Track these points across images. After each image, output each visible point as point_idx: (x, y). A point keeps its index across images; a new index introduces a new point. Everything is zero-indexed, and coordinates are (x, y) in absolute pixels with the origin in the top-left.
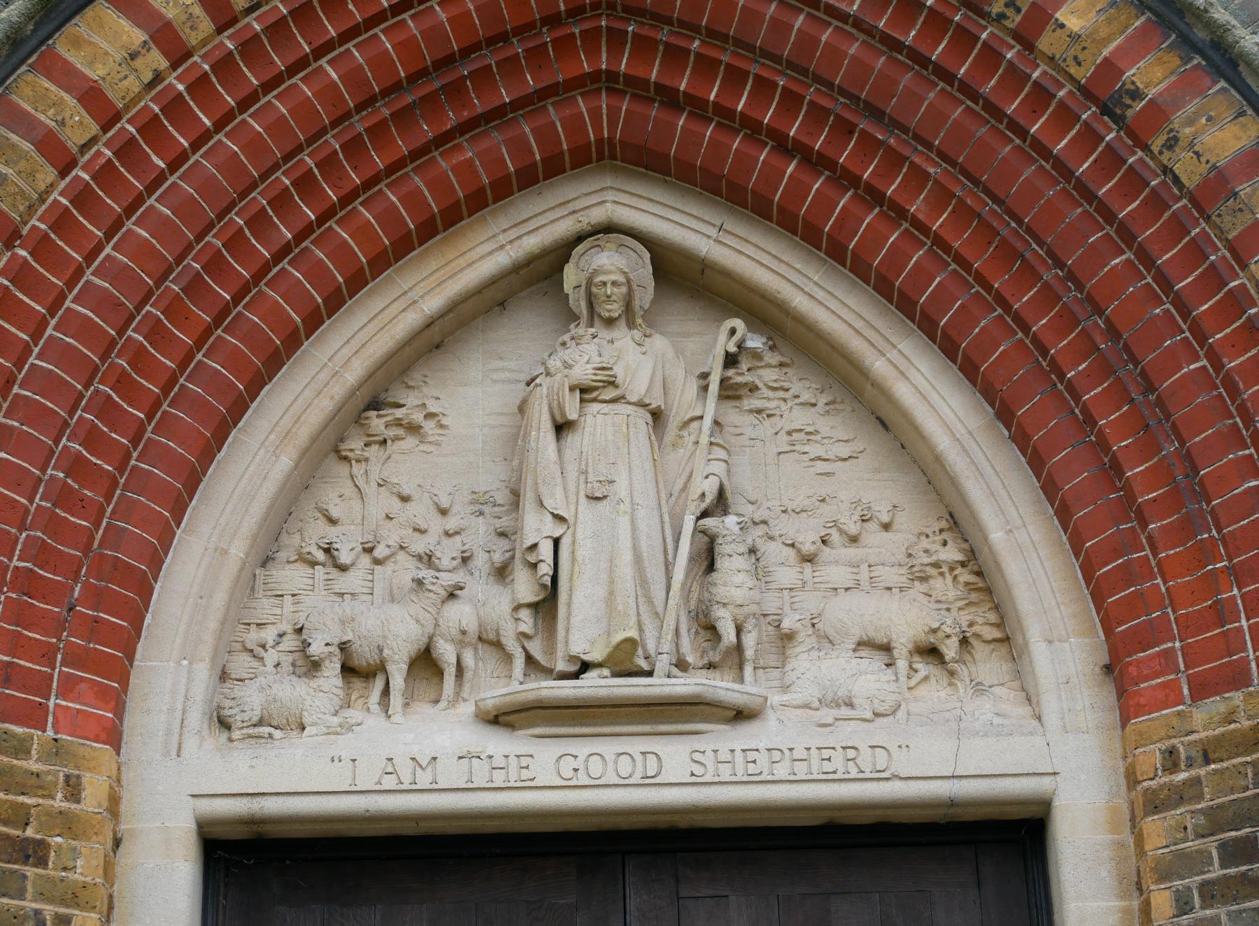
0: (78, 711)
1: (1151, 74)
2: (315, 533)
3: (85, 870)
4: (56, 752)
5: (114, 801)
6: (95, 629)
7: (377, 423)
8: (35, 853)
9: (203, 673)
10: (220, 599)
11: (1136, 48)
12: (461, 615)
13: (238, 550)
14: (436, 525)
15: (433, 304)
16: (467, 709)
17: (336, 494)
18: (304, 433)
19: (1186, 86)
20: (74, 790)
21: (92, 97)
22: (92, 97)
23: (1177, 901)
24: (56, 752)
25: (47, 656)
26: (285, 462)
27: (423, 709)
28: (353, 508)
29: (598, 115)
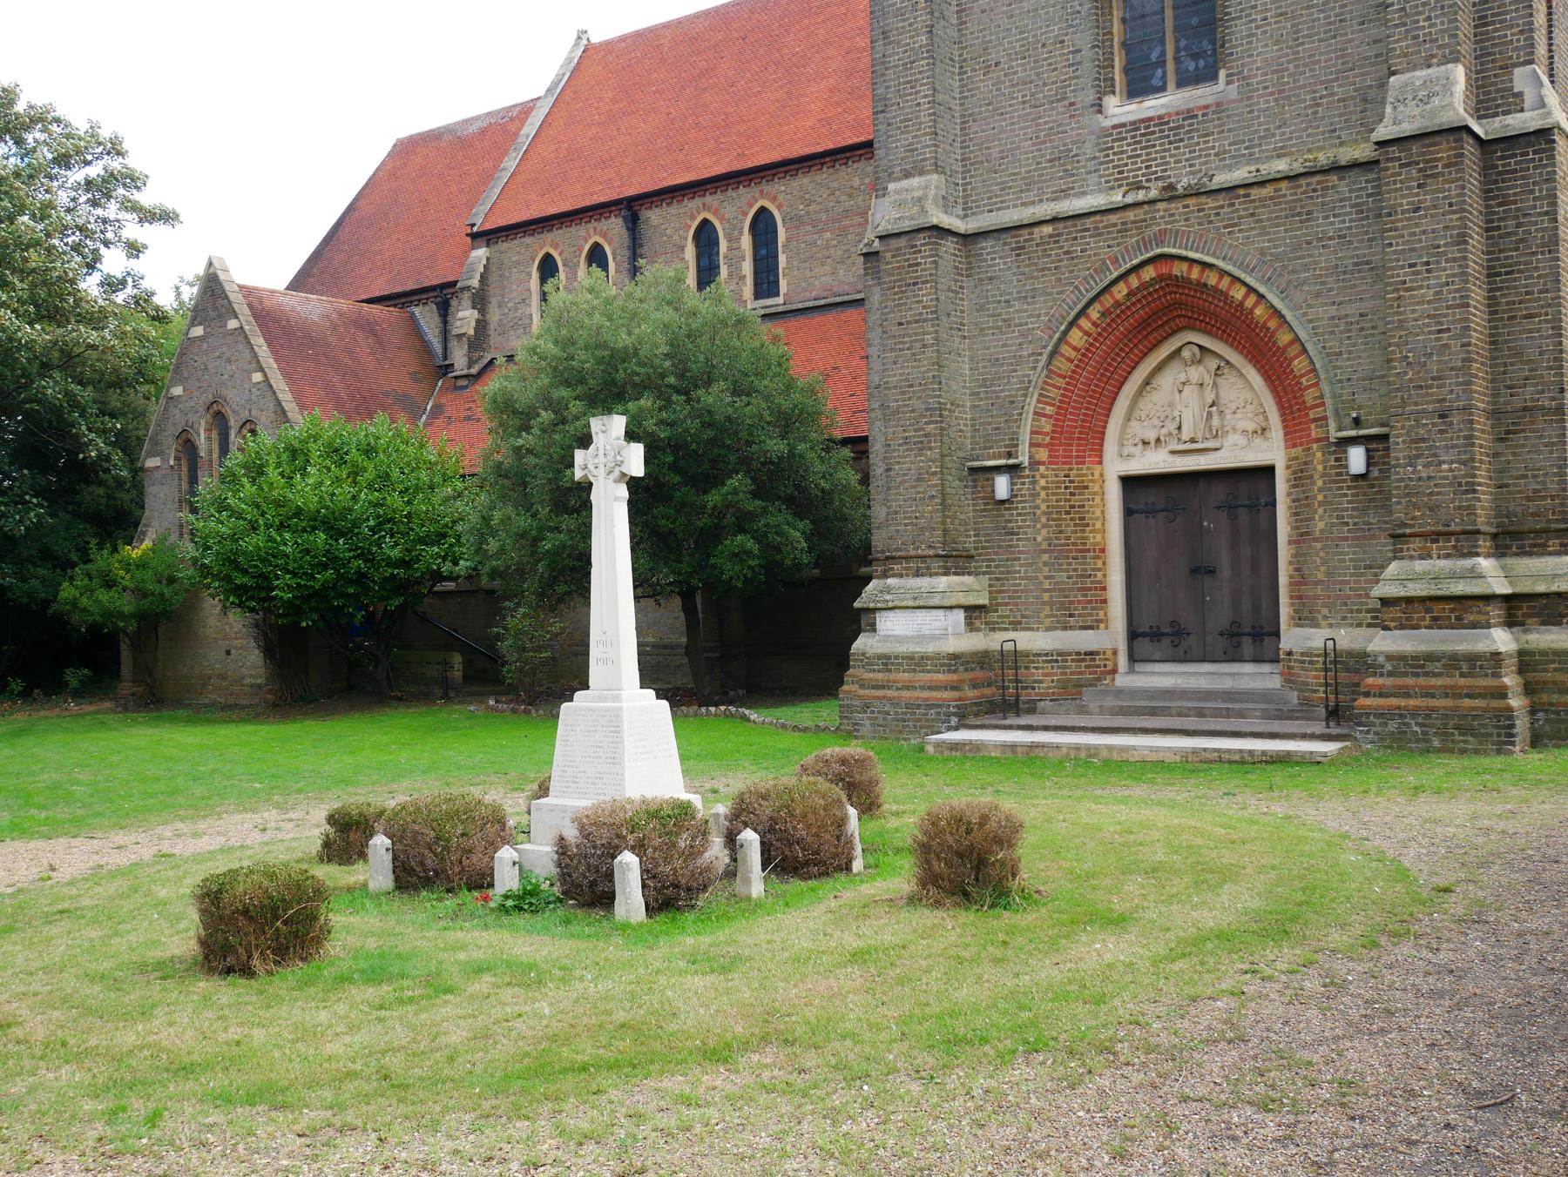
1: (1272, 324)
2: (1136, 414)
3: (1097, 489)
5: (1102, 475)
8: (1086, 487)
11: (1269, 318)
12: (1164, 431)
17: (1141, 405)
19: (1280, 326)
21: (1075, 349)
22: (1075, 349)
23: (146, 705)
28: (1145, 406)
29: (1182, 322)
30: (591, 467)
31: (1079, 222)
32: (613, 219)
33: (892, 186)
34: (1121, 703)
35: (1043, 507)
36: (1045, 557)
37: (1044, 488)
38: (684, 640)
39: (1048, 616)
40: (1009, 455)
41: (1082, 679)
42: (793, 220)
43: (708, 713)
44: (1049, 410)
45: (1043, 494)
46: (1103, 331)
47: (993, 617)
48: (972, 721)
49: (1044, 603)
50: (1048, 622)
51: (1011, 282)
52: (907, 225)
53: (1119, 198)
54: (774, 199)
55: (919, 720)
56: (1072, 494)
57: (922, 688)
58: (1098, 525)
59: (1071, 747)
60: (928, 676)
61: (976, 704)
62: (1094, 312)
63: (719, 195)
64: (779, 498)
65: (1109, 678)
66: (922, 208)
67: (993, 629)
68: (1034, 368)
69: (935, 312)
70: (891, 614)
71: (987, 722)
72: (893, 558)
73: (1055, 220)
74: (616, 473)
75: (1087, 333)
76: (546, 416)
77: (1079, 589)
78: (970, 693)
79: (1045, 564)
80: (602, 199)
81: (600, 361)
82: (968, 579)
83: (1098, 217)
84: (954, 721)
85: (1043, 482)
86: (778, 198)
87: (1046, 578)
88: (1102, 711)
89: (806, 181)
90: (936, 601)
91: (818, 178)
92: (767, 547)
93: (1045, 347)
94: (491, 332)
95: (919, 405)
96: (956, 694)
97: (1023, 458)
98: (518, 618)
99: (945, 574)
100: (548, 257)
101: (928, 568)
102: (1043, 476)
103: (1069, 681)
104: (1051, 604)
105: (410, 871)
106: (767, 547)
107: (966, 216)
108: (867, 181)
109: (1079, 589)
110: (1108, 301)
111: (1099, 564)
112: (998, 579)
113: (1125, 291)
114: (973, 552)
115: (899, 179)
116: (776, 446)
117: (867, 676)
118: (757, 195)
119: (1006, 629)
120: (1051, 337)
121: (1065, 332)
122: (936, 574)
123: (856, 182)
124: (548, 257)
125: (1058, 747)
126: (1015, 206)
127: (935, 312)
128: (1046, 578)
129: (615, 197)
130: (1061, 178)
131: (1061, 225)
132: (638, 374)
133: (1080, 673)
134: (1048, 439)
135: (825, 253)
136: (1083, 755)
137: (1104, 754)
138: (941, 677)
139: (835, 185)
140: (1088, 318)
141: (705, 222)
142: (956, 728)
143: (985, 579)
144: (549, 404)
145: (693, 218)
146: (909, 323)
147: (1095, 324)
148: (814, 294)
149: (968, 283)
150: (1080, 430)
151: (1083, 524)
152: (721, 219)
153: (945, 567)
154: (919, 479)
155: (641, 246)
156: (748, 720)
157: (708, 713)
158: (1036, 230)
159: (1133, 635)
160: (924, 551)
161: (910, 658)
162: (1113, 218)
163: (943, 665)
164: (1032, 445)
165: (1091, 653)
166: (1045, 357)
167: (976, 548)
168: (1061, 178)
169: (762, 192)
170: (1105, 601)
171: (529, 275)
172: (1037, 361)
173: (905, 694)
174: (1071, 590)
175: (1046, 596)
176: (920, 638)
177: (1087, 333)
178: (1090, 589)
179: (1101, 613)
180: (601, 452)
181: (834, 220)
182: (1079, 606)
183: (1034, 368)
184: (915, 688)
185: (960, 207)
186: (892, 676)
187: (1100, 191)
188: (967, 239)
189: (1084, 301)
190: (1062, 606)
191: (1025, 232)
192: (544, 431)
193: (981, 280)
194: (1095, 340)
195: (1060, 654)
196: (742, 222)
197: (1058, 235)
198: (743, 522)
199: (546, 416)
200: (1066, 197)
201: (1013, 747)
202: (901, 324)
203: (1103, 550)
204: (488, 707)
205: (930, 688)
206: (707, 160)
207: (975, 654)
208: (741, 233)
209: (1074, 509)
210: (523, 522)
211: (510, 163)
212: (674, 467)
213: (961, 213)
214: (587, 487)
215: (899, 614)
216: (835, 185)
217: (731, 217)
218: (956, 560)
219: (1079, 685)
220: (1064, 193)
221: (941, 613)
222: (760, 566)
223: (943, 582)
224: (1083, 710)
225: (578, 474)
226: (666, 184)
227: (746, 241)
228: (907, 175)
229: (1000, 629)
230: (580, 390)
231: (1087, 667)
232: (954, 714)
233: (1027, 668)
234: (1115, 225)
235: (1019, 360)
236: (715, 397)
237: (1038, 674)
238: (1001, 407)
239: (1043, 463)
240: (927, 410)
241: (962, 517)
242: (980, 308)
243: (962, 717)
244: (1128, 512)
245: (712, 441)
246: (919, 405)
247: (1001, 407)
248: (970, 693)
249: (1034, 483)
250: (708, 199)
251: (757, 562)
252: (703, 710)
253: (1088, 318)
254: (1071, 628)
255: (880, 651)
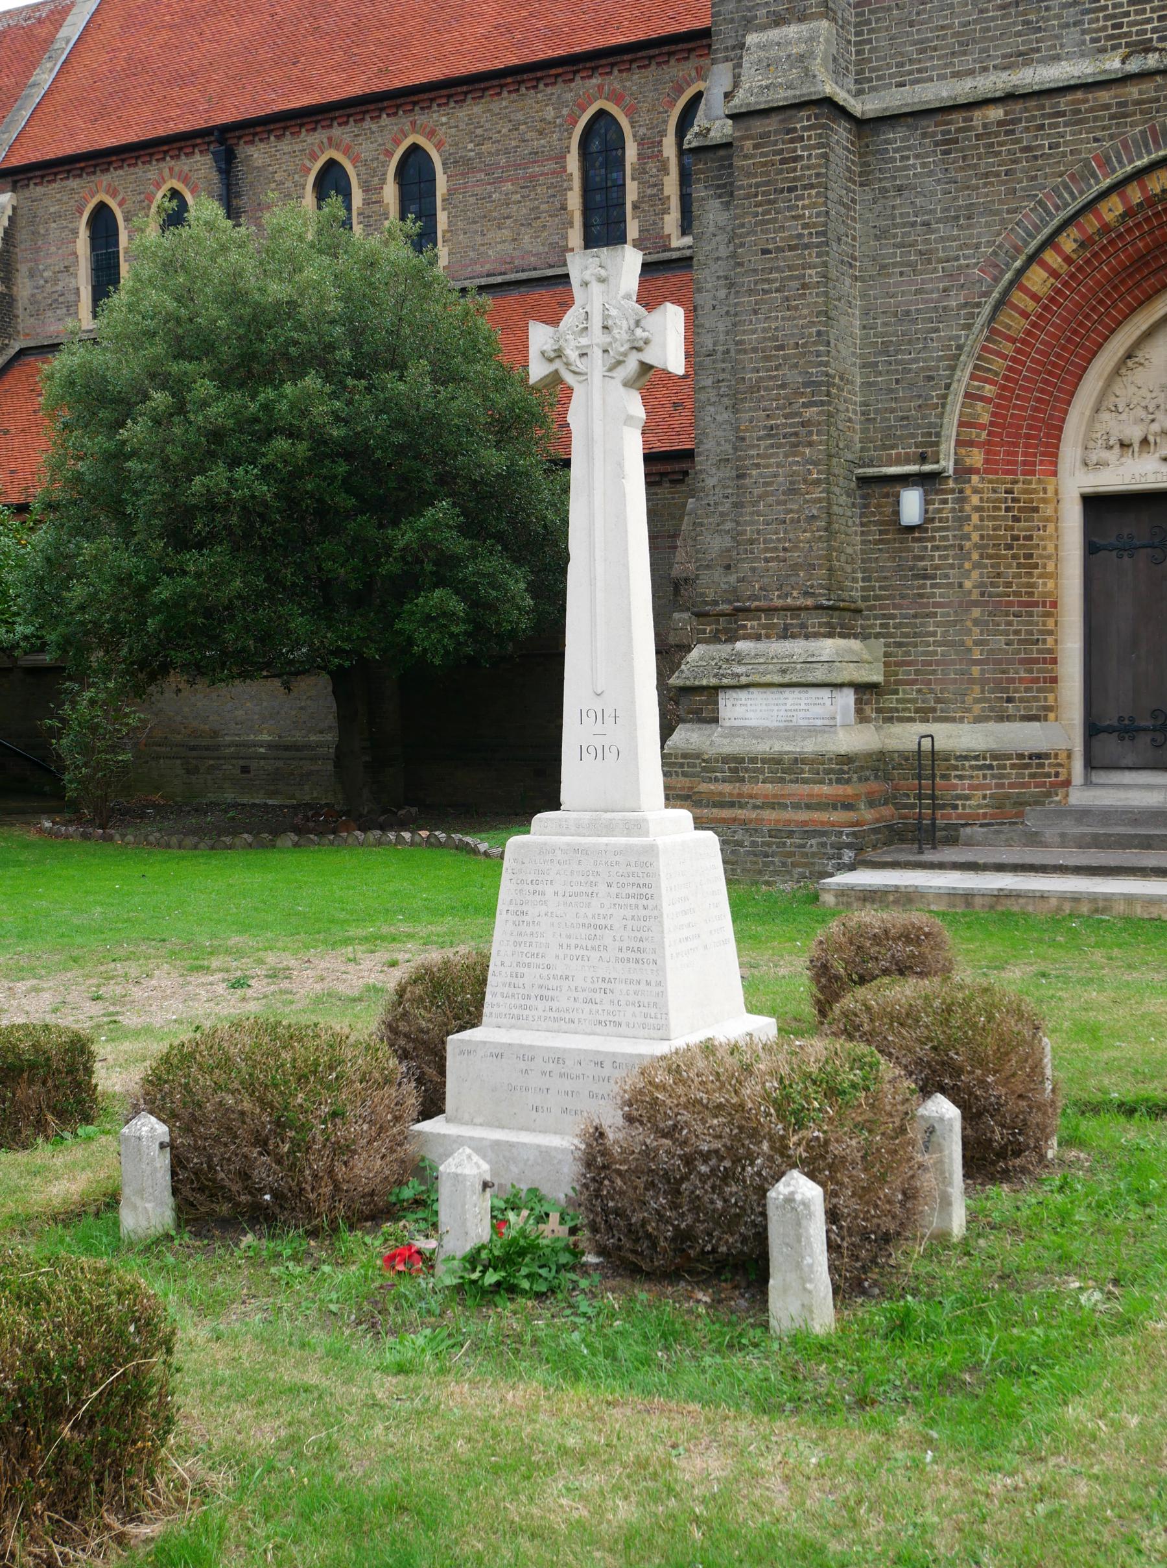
0: (953, 896)
2: (1110, 401)
3: (1049, 512)
4: (1040, 481)
5: (1056, 492)
6: (1048, 445)
7: (1130, 363)
9: (1079, 451)
10: (1083, 428)
13: (1088, 413)
14: (1149, 395)
15: (1144, 327)
16: (1157, 455)
17: (1118, 389)
18: (1106, 374)
20: (1045, 491)
21: (1035, 297)
22: (1035, 297)
24: (1040, 481)
25: (1035, 455)
26: (1101, 384)
27: (1145, 455)
28: (1124, 391)
30: (572, 354)
31: (1047, 103)
32: (197, 157)
33: (752, 39)
34: (1089, 830)
35: (975, 537)
36: (976, 612)
37: (978, 509)
38: (331, 737)
39: (977, 701)
40: (923, 459)
41: (1023, 795)
42: (459, 165)
43: (400, 841)
44: (989, 390)
45: (975, 517)
46: (1078, 270)
47: (891, 701)
48: (870, 855)
49: (972, 681)
50: (977, 708)
51: (933, 193)
52: (781, 97)
53: (1117, 64)
54: (430, 135)
55: (793, 854)
56: (1016, 519)
57: (796, 806)
58: (1050, 567)
59: (1063, 897)
60: (805, 789)
61: (875, 831)
62: (1068, 243)
63: (352, 128)
64: (490, 536)
65: (1061, 792)
66: (807, 70)
67: (890, 720)
68: (969, 327)
69: (824, 234)
70: (743, 695)
71: (903, 857)
72: (747, 610)
73: (1010, 97)
74: (631, 366)
75: (1054, 274)
76: (160, 399)
77: (1022, 661)
78: (868, 815)
79: (976, 622)
80: (182, 128)
81: (238, 320)
82: (855, 644)
83: (1079, 95)
84: (848, 856)
85: (975, 500)
86: (438, 134)
87: (977, 643)
88: (1064, 841)
89: (477, 109)
90: (819, 675)
91: (495, 106)
92: (477, 605)
93: (986, 294)
94: (20, 312)
95: (793, 377)
96: (851, 816)
97: (947, 464)
98: (84, 703)
99: (830, 635)
100: (102, 207)
101: (803, 626)
102: (976, 491)
103: (1008, 796)
104: (983, 682)
105: (214, 1191)
106: (477, 605)
107: (860, 92)
108: (565, 112)
109: (1022, 661)
110: (1091, 224)
111: (1050, 622)
112: (899, 645)
113: (1120, 209)
114: (860, 604)
115: (764, 28)
116: (494, 459)
117: (704, 787)
118: (407, 128)
119: (910, 720)
120: (996, 280)
121: (1020, 272)
122: (816, 635)
123: (550, 113)
124: (102, 207)
125: (1043, 897)
126: (941, 77)
127: (824, 234)
128: (977, 643)
129: (201, 124)
130: (1019, 34)
131: (1018, 106)
132: (296, 343)
133: (1023, 785)
134: (984, 434)
135: (505, 211)
136: (1085, 909)
137: (1120, 907)
138: (826, 789)
139: (520, 116)
140: (1058, 250)
141: (332, 164)
142: (852, 867)
143: (879, 645)
144: (163, 381)
145: (314, 157)
146: (780, 250)
147: (1068, 260)
148: (487, 267)
149: (864, 195)
150: (1028, 426)
151: (1029, 563)
152: (355, 161)
153: (828, 624)
154: (792, 491)
155: (239, 195)
156: (474, 851)
157: (400, 841)
158: (977, 114)
159: (1092, 729)
160: (796, 599)
161: (775, 761)
162: (1104, 96)
163: (829, 772)
164: (959, 443)
165: (1039, 756)
166: (987, 310)
167: (865, 599)
168: (1019, 34)
169: (413, 123)
170: (1054, 680)
171: (75, 232)
172: (972, 316)
173: (768, 814)
174: (1010, 662)
175: (976, 670)
176: (791, 731)
177: (1054, 274)
178: (1035, 661)
179: (1051, 696)
180: (596, 322)
181: (517, 166)
182: (1019, 689)
183: (969, 327)
184: (784, 807)
185: (851, 78)
186: (746, 788)
187: (1083, 55)
188: (862, 125)
189: (1056, 222)
190: (999, 687)
191: (957, 117)
192: (157, 422)
193: (884, 190)
194: (1065, 283)
195: (995, 757)
196: (385, 164)
197: (1013, 122)
198: (445, 570)
199: (160, 399)
200: (1026, 64)
201: (968, 897)
202: (765, 252)
203: (1054, 604)
204: (41, 831)
205: (808, 807)
206: (334, 78)
207: (869, 755)
208: (383, 181)
209: (1017, 542)
210: (127, 561)
211: (44, 77)
212: (347, 485)
213: (853, 87)
214: (557, 390)
215: (757, 695)
216: (520, 116)
217: (371, 156)
218: (841, 617)
219: (1021, 803)
220: (1024, 57)
221: (825, 693)
222: (466, 632)
223: (828, 647)
224: (1034, 839)
225: (537, 371)
226: (276, 108)
227: (390, 193)
228: (778, 21)
229: (901, 720)
230: (206, 366)
231: (1032, 776)
232: (849, 846)
233: (945, 777)
234: (1107, 107)
235: (943, 314)
236: (413, 385)
237: (961, 787)
238: (912, 385)
239: (976, 471)
240: (806, 384)
241: (849, 550)
242: (882, 234)
243: (859, 849)
244: (1091, 549)
245: (400, 450)
246: (793, 377)
247: (912, 385)
248: (868, 815)
249: (962, 500)
250: (336, 131)
251: (463, 627)
252: (392, 836)
253: (1058, 250)
254: (1009, 718)
255: (727, 750)
